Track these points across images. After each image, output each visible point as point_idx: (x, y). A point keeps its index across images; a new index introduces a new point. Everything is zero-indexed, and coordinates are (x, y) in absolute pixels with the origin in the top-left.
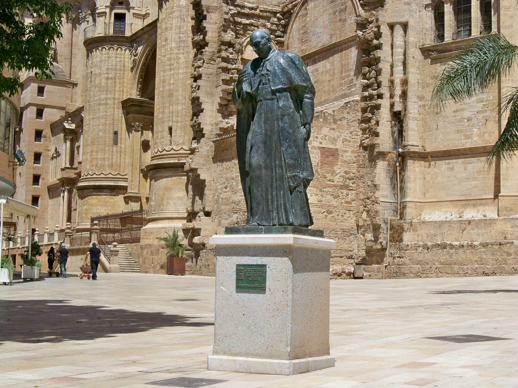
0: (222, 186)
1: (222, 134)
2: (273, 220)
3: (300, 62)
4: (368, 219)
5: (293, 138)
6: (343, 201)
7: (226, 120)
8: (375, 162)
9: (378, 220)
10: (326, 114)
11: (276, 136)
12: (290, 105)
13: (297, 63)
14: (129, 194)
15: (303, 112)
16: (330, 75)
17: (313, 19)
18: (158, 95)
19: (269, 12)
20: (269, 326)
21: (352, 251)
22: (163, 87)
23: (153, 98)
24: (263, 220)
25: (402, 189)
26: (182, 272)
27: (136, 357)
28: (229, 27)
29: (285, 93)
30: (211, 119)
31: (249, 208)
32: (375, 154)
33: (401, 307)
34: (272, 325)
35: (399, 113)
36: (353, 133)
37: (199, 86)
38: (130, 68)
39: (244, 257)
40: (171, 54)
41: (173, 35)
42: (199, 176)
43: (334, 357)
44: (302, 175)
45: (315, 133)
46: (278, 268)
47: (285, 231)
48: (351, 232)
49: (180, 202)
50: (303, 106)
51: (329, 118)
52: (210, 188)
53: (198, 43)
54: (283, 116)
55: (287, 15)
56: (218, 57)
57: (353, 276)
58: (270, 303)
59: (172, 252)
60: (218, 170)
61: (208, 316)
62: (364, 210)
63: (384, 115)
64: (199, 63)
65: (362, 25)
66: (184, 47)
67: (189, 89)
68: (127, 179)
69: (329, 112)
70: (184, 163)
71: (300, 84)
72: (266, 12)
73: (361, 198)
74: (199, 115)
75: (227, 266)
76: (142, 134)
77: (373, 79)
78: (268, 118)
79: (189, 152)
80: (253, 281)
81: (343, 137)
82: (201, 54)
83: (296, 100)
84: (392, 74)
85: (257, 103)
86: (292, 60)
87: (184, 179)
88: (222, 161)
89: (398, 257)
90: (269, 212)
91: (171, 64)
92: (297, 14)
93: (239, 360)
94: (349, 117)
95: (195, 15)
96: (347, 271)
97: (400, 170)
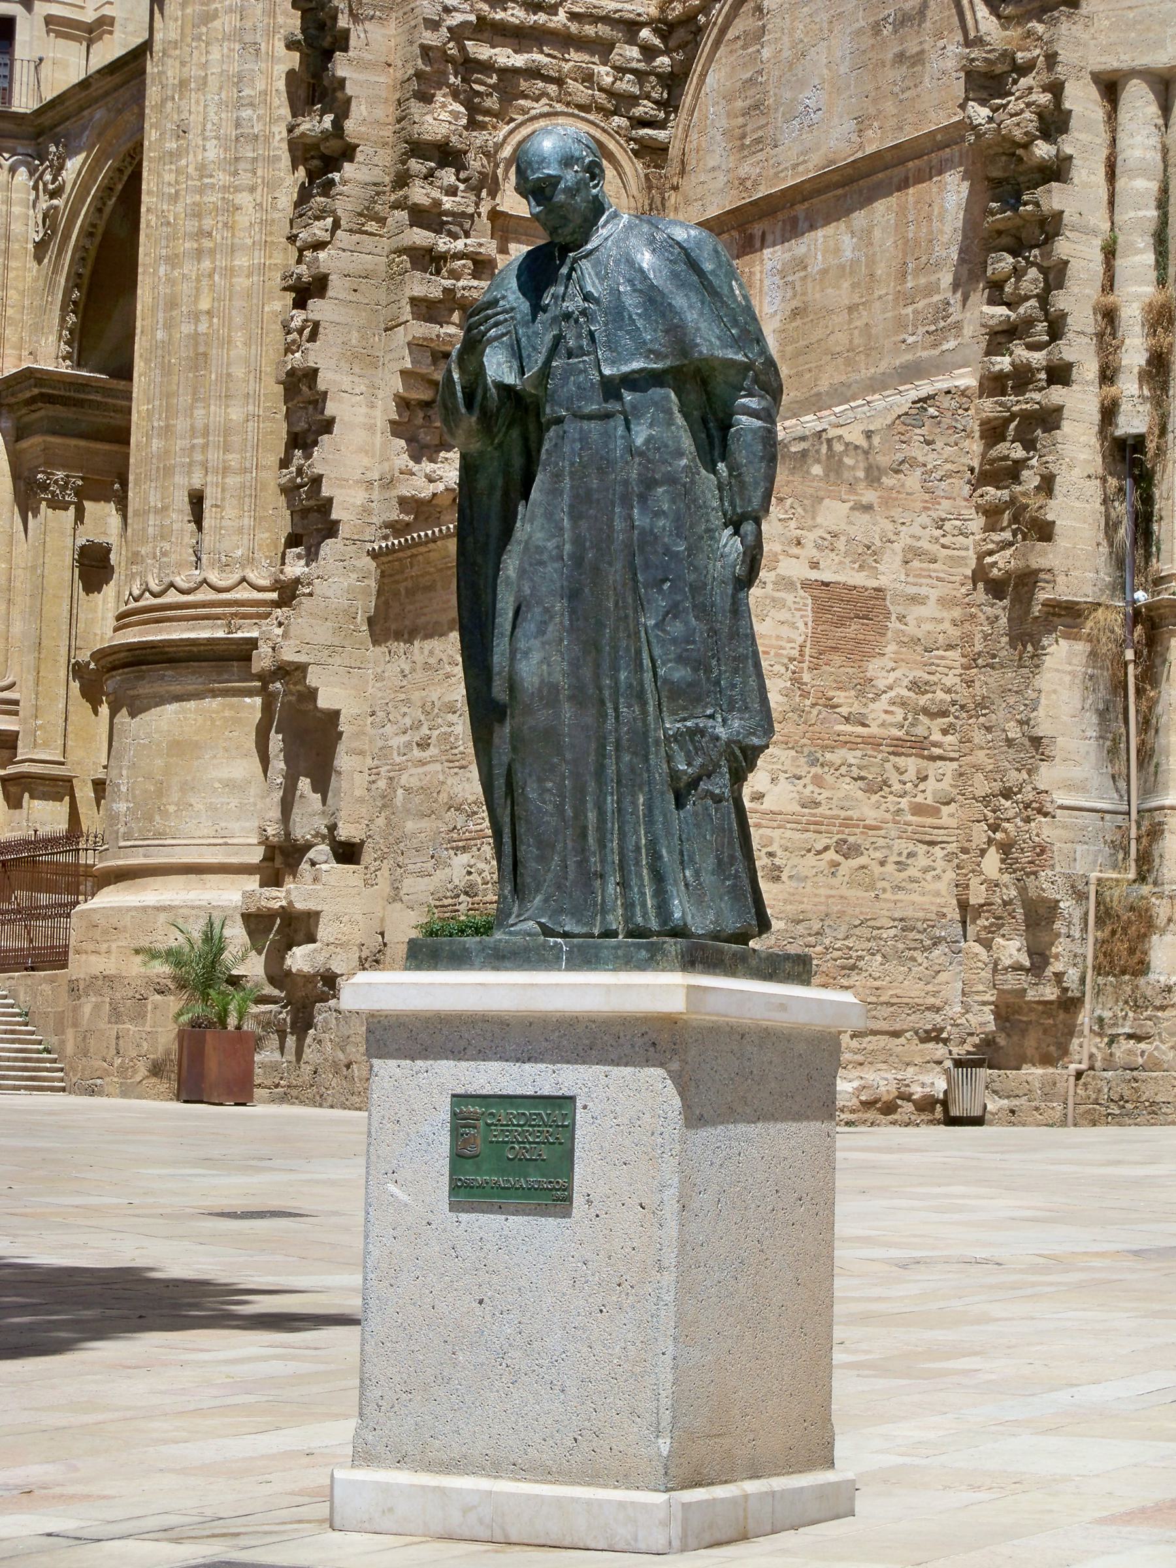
0: (406, 738)
1: (408, 524)
2: (604, 912)
3: (720, 266)
4: (1006, 878)
5: (691, 577)
6: (904, 803)
7: (427, 466)
8: (1037, 645)
9: (1049, 885)
10: (838, 447)
11: (619, 565)
12: (677, 439)
13: (708, 266)
14: (25, 768)
15: (731, 469)
16: (854, 286)
17: (787, 53)
18: (147, 361)
19: (606, 19)
20: (585, 1349)
21: (938, 1010)
22: (169, 326)
23: (125, 372)
24: (562, 911)
25: (1146, 755)
26: (240, 1091)
27: (33, 1472)
28: (441, 83)
29: (656, 392)
30: (366, 461)
31: (508, 861)
32: (1036, 610)
33: (1137, 1253)
34: (598, 1347)
35: (1139, 442)
36: (948, 526)
37: (316, 325)
38: (31, 246)
39: (482, 1065)
40: (201, 190)
41: (212, 110)
42: (312, 694)
43: (850, 1475)
44: (726, 729)
45: (793, 524)
46: (621, 1115)
47: (652, 960)
48: (937, 932)
49: (234, 802)
50: (733, 446)
51: (848, 461)
52: (356, 744)
53: (316, 146)
54: (649, 484)
55: (681, 34)
56: (396, 206)
57: (945, 1113)
58: (589, 1255)
59: (198, 1009)
60: (392, 670)
61: (335, 1288)
62: (990, 841)
63: (1077, 449)
64: (319, 229)
65: (988, 82)
66: (255, 160)
67: (276, 337)
68: (16, 703)
69: (848, 438)
70: (253, 643)
71: (720, 353)
72: (596, 19)
73: (980, 793)
74: (316, 443)
75: (419, 1095)
76: (80, 517)
77: (1033, 302)
78: (589, 492)
79: (274, 595)
80: (521, 1164)
81: (904, 540)
82: (325, 193)
83: (704, 421)
84: (1109, 284)
85: (542, 429)
86: (688, 255)
87: (252, 707)
88: (408, 634)
89: (1130, 1036)
90: (588, 878)
91: (202, 234)
92: (723, 31)
93: (459, 1491)
94: (932, 460)
95: (304, 30)
96: (918, 1092)
97: (1142, 678)
